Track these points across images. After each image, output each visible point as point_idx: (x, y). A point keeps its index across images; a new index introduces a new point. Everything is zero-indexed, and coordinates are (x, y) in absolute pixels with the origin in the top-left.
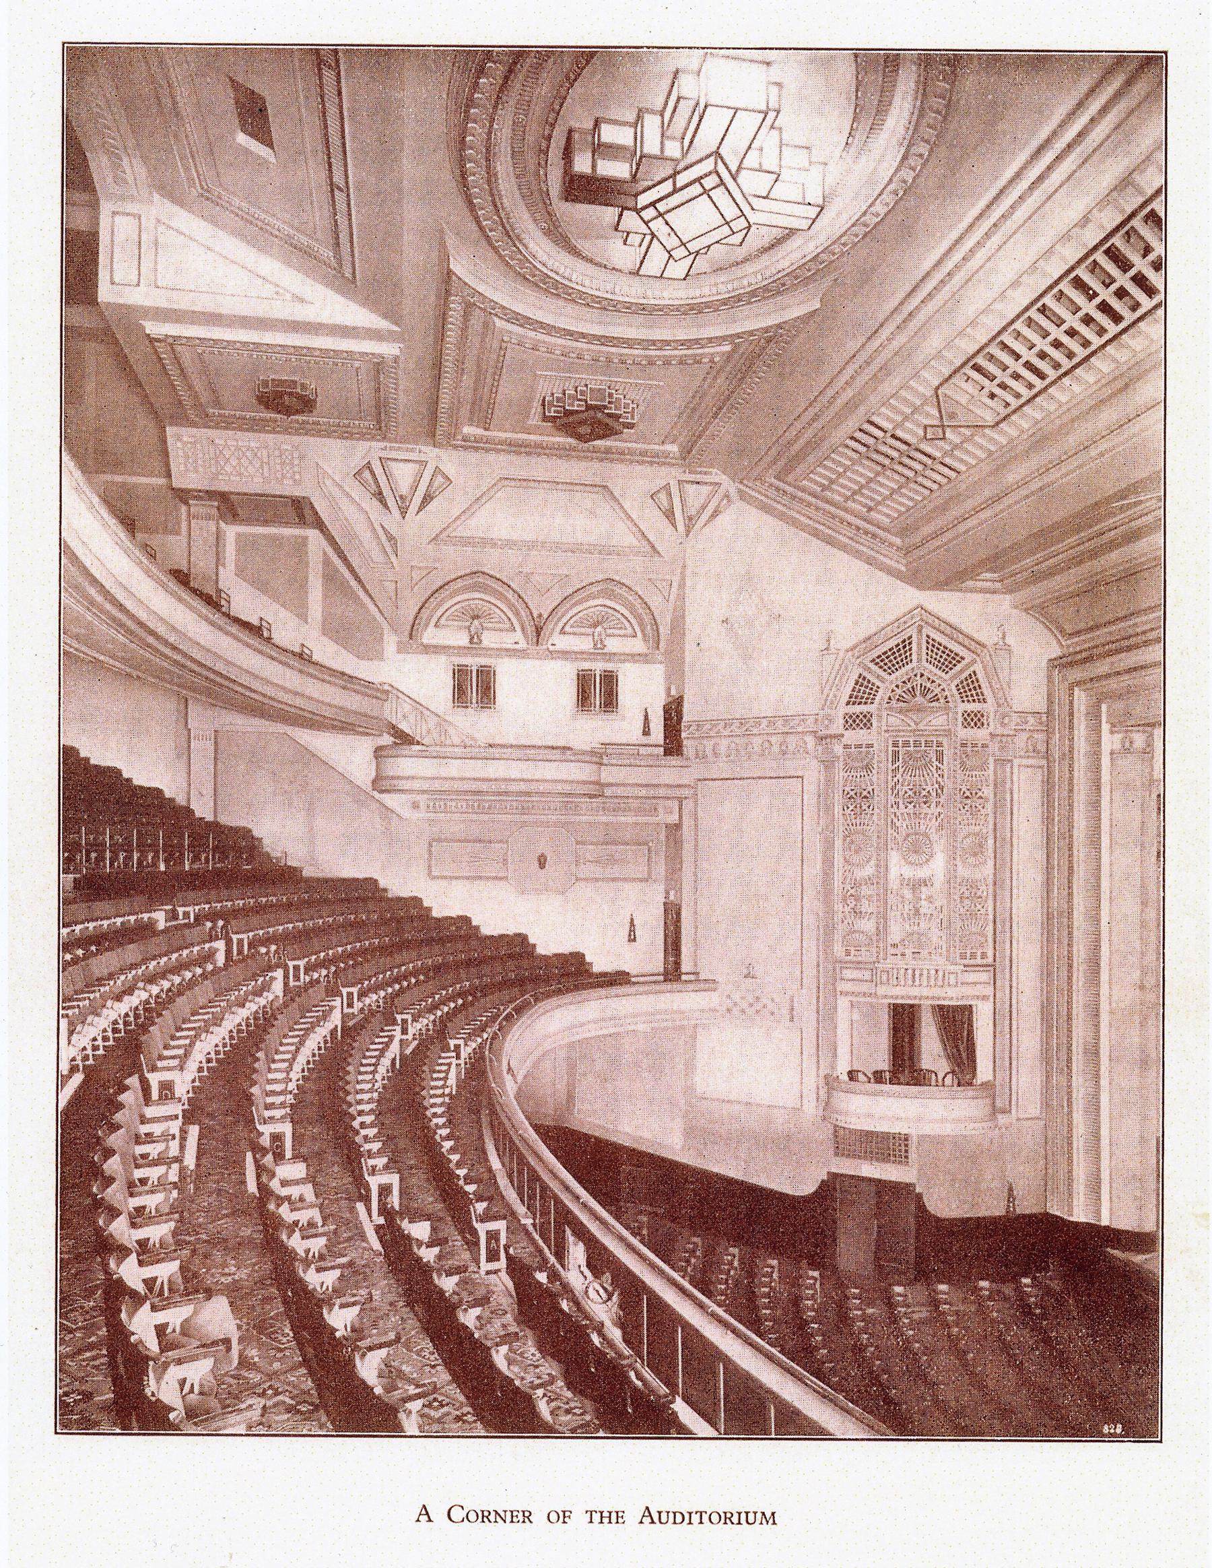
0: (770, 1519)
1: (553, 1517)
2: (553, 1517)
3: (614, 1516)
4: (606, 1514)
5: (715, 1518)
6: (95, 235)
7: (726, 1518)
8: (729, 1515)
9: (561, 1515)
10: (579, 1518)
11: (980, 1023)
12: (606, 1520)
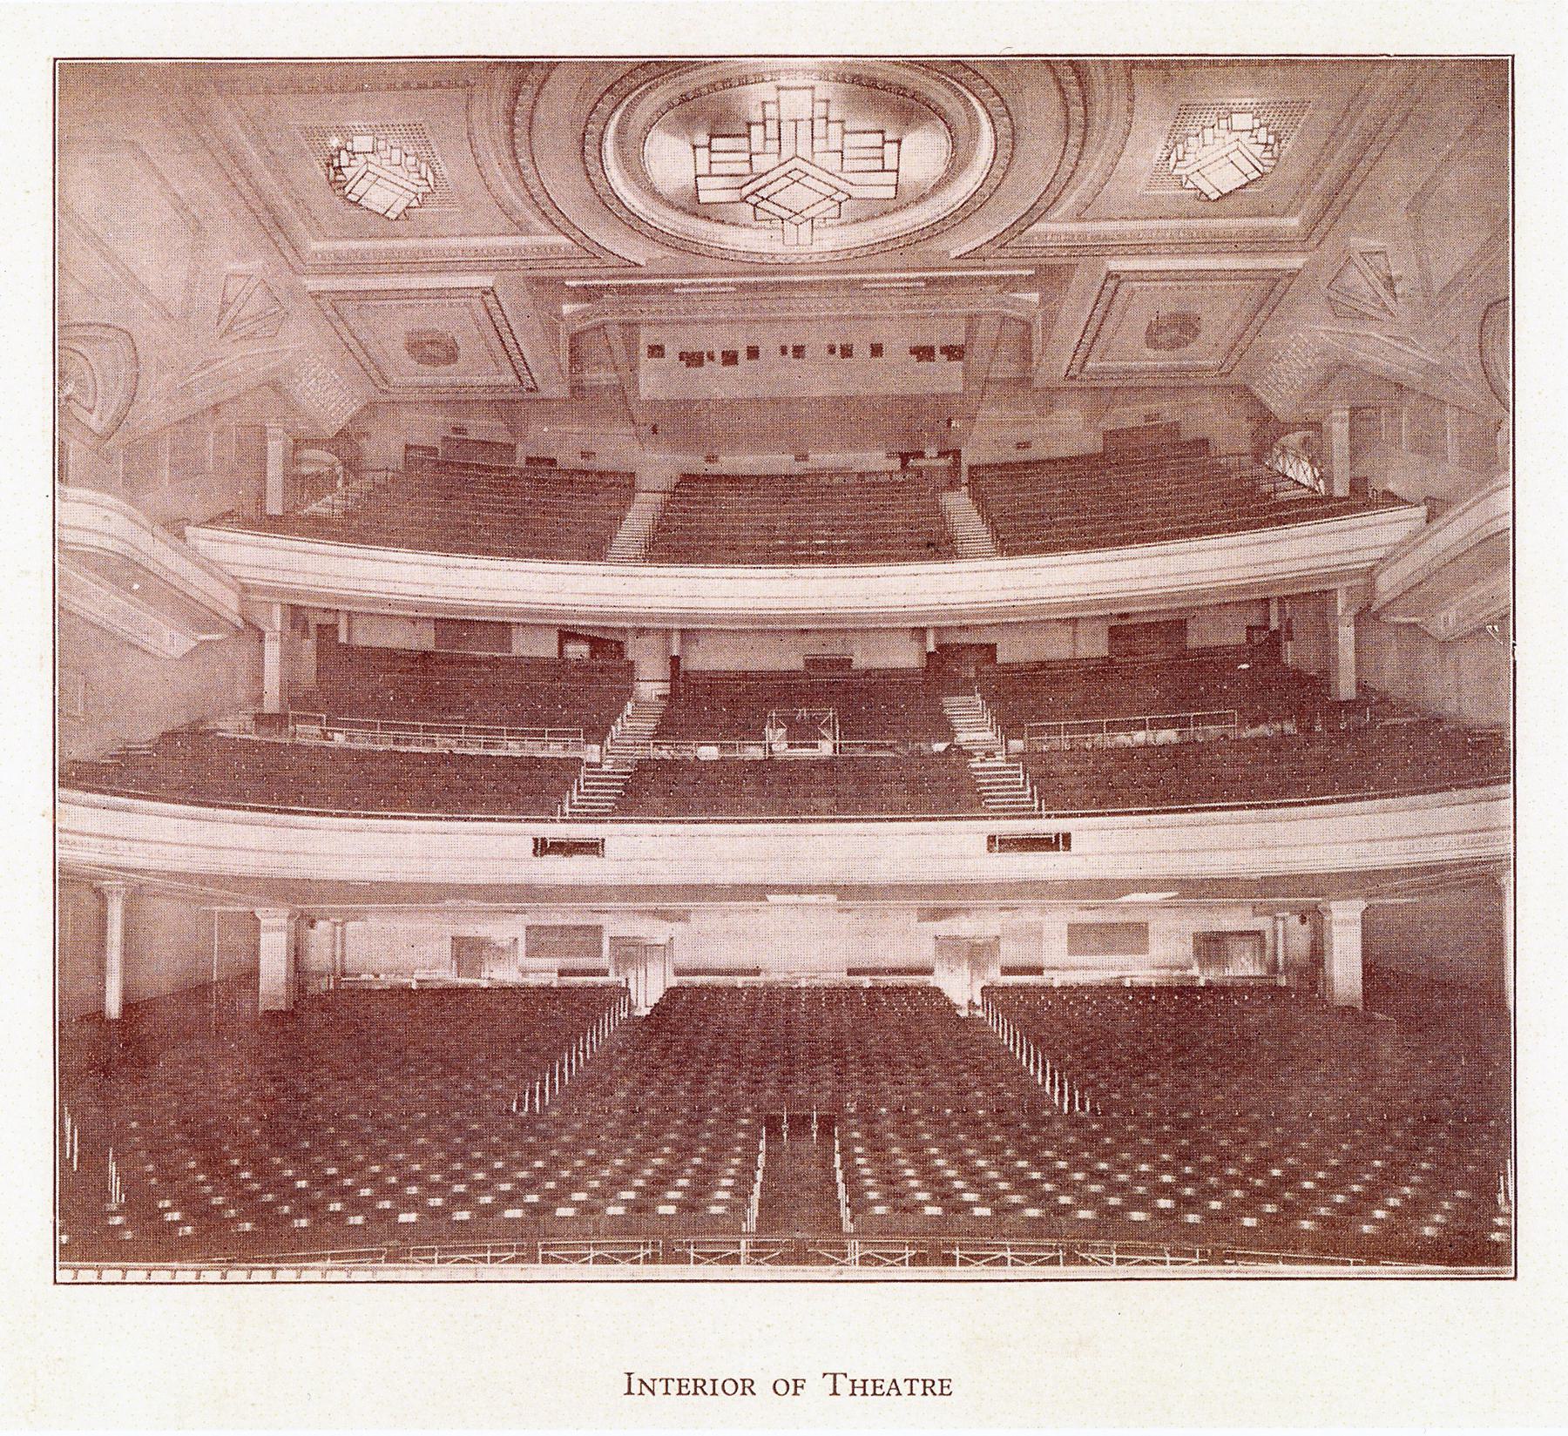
0: (937, 1387)
1: (781, 1387)
2: (781, 1387)
3: (869, 1385)
4: (859, 1383)
5: (730, 1387)
6: (959, 556)
7: (699, 1387)
8: (700, 1383)
9: (740, 1384)
10: (817, 1388)
11: (891, 956)
12: (859, 1391)
